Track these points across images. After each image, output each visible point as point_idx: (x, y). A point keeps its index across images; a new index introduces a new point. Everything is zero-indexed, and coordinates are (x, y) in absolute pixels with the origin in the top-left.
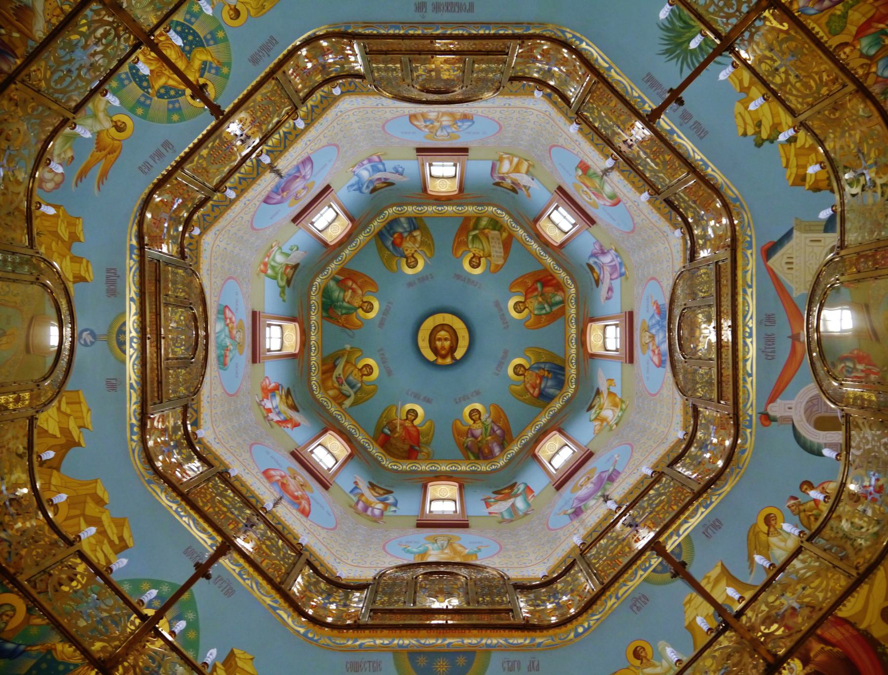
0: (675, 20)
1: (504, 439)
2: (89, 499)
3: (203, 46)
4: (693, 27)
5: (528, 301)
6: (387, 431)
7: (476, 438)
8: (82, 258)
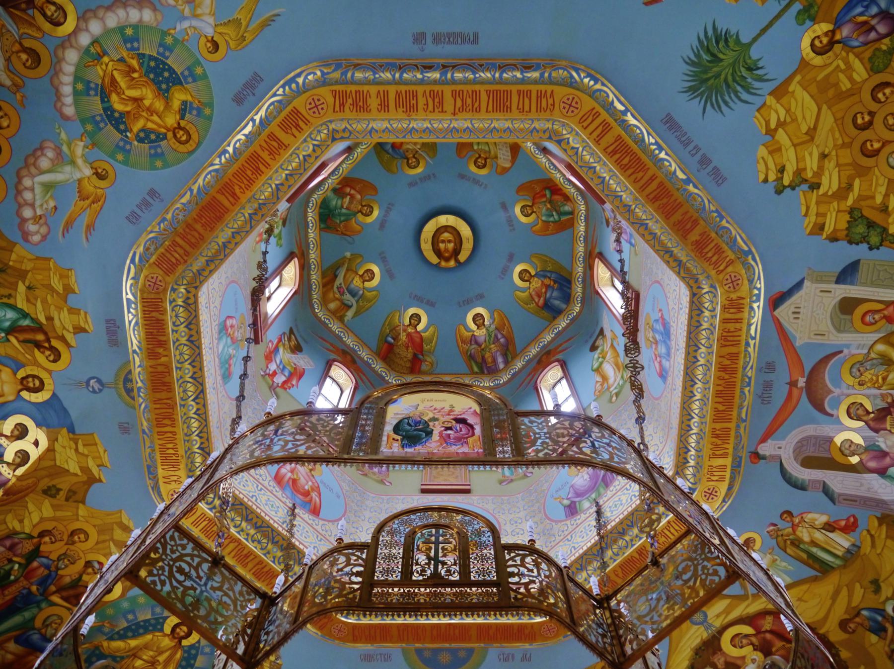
0: (702, 52)
1: (507, 349)
2: (115, 527)
3: (181, 84)
4: (721, 60)
5: (536, 206)
6: (390, 339)
7: (479, 345)
8: (79, 310)
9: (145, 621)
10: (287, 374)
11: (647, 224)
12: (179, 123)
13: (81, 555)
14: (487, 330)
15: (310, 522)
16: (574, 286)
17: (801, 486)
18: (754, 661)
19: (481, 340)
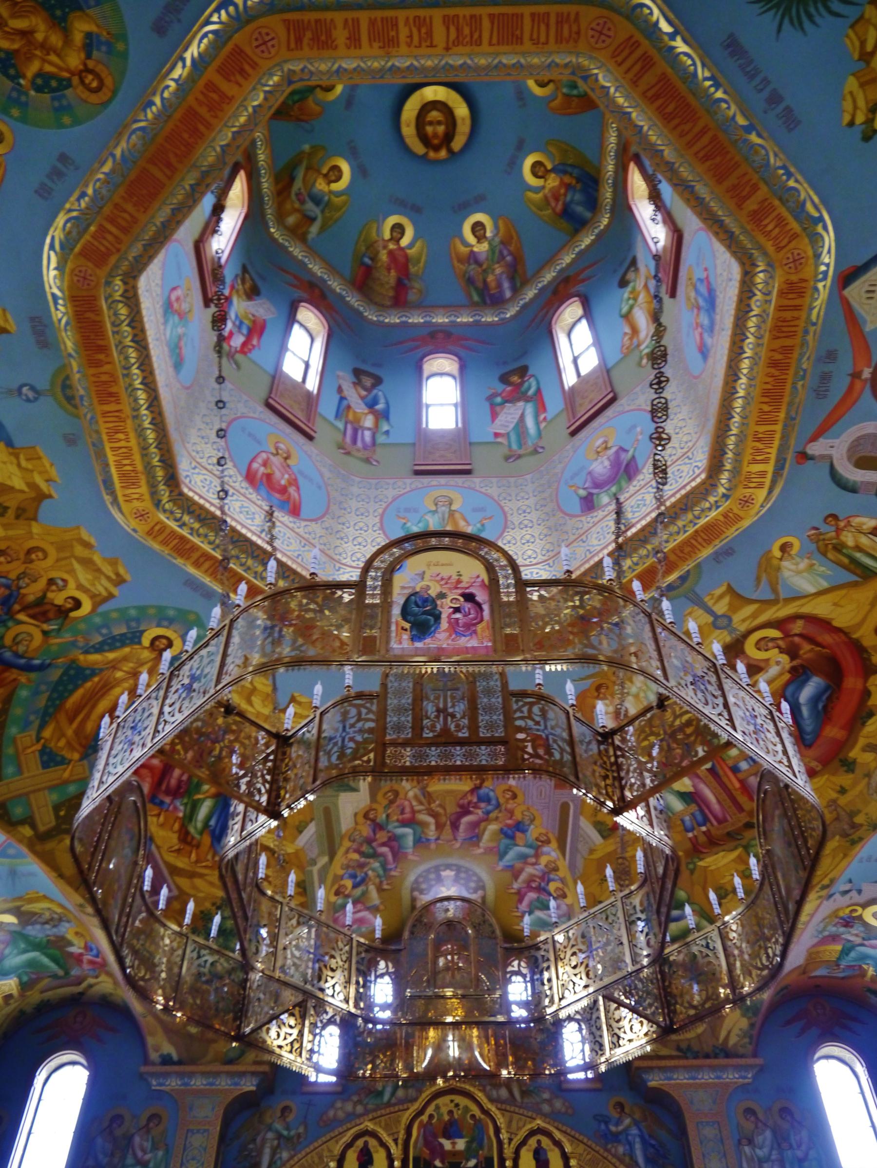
2: (75, 543)
6: (367, 260)
9: (122, 635)
10: (245, 331)
11: (693, 187)
12: (85, 65)
13: (42, 573)
14: (490, 244)
15: (291, 525)
16: (602, 190)
17: (851, 488)
18: (778, 663)
19: (482, 257)
